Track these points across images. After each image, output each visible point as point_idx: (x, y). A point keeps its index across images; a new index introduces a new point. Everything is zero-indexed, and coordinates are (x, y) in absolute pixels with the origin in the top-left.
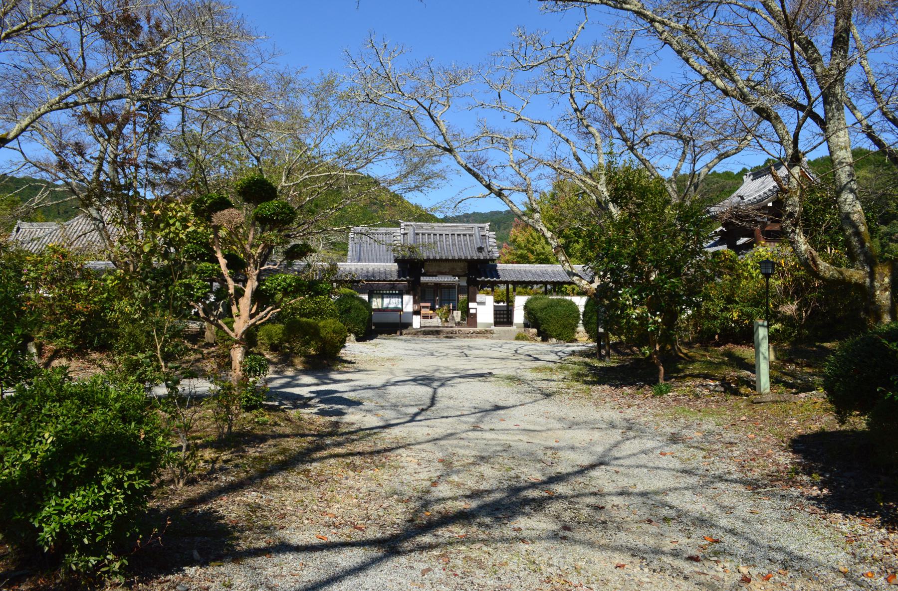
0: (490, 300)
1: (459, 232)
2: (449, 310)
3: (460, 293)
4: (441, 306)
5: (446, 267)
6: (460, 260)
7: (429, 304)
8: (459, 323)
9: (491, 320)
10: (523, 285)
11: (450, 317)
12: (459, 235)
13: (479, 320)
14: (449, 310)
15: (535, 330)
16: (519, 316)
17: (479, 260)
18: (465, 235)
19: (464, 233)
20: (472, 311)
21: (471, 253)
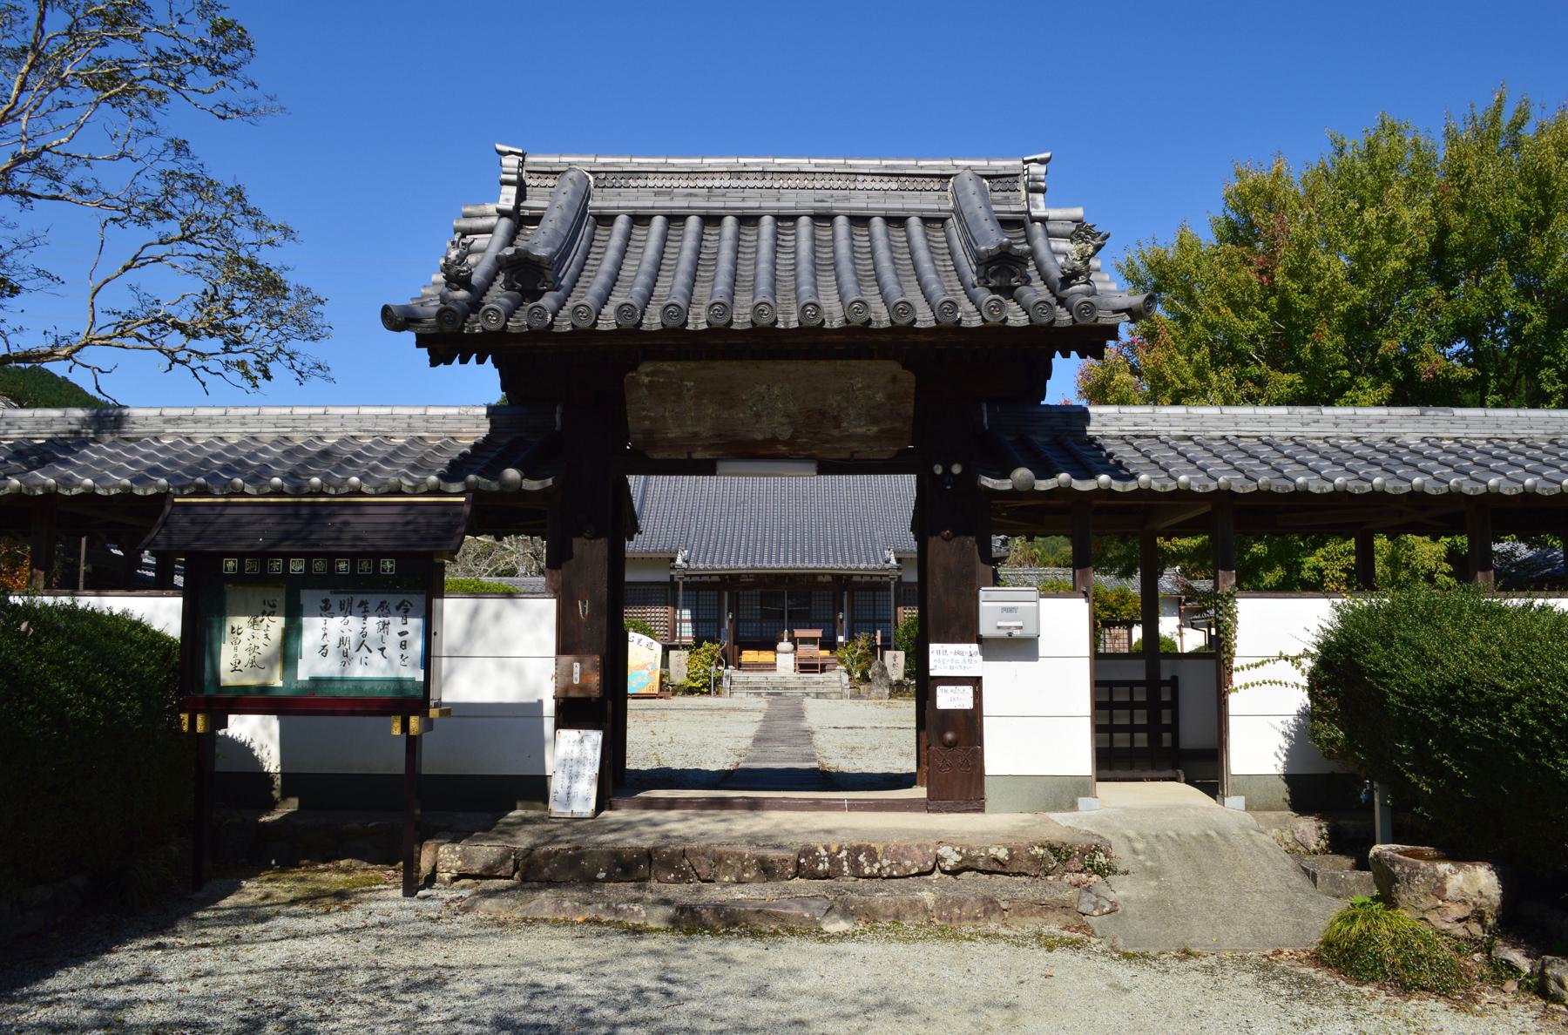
0: (1065, 623)
1: (859, 203)
2: (873, 649)
3: (901, 601)
4: (851, 637)
5: (773, 394)
6: (857, 341)
7: (818, 633)
8: (899, 683)
9: (1073, 751)
10: (1260, 534)
11: (875, 668)
12: (859, 221)
13: (1004, 753)
14: (873, 649)
15: (1478, 882)
16: (1263, 723)
17: (997, 332)
18: (896, 221)
19: (895, 205)
20: (949, 699)
21: (933, 289)
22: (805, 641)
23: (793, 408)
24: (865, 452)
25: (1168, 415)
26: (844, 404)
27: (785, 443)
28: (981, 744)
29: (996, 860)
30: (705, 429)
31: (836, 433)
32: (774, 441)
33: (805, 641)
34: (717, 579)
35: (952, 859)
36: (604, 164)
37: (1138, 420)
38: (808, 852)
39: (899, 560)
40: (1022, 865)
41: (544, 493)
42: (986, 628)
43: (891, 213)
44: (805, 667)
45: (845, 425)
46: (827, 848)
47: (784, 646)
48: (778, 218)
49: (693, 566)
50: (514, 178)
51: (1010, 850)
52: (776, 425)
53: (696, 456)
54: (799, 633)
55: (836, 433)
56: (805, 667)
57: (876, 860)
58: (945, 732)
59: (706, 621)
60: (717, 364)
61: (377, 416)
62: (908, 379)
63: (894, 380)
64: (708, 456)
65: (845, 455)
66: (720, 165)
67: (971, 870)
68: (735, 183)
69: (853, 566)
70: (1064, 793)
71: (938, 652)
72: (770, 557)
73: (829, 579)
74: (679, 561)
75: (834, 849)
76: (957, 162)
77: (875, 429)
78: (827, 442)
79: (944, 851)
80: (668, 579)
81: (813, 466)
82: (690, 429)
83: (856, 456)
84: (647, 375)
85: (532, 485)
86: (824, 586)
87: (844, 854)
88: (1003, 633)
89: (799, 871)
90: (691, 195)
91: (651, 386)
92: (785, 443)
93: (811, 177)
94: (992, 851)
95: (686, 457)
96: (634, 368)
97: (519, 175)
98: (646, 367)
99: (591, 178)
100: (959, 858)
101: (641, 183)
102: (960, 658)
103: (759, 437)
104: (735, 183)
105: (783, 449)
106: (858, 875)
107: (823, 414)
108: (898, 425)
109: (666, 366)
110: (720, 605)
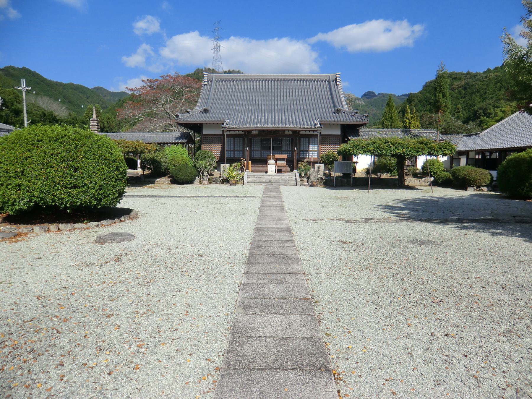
7: (285, 156)
22: (280, 159)
33: (280, 159)
44: (279, 171)
47: (272, 161)
49: (230, 126)
54: (277, 156)
56: (279, 171)
73: (290, 133)
86: (288, 136)
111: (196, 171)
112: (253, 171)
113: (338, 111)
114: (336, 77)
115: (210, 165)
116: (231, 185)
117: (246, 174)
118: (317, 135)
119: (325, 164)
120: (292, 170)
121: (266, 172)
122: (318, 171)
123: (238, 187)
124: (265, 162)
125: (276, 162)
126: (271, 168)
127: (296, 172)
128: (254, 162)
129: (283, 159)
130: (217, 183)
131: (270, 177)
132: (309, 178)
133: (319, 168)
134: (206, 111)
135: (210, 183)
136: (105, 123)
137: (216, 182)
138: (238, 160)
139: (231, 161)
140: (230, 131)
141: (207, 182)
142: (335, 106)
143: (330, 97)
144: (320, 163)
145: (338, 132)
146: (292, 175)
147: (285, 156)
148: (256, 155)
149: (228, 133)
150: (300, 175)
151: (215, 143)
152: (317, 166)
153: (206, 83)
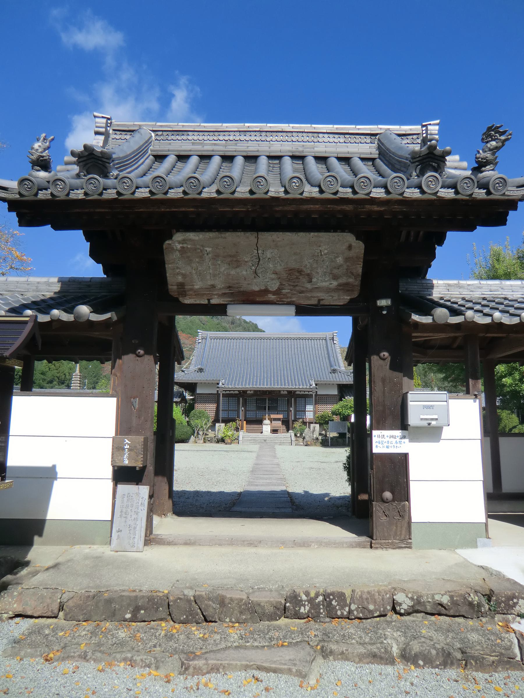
0: (464, 414)
7: (281, 416)
9: (469, 502)
22: (275, 419)
23: (279, 268)
24: (329, 300)
25: (511, 286)
26: (315, 265)
27: (274, 293)
28: (408, 499)
29: (441, 605)
30: (219, 283)
31: (309, 286)
32: (266, 291)
33: (275, 419)
34: (237, 392)
35: (405, 602)
36: (161, 126)
37: (493, 288)
38: (294, 598)
39: (316, 385)
40: (463, 610)
41: (106, 323)
42: (413, 420)
43: (339, 156)
44: (275, 431)
45: (314, 280)
46: (307, 594)
47: (267, 422)
48: (270, 157)
49: (226, 386)
50: (103, 130)
51: (452, 597)
52: (268, 281)
53: (213, 302)
54: (273, 416)
55: (309, 286)
56: (275, 431)
57: (346, 605)
58: (383, 491)
59: (232, 410)
60: (228, 234)
61: (18, 282)
62: (359, 247)
63: (350, 247)
64: (224, 303)
65: (314, 302)
66: (233, 127)
67: (418, 612)
68: (243, 138)
69: (297, 387)
70: (465, 535)
71: (379, 436)
72: (260, 383)
73: (286, 393)
74: (220, 384)
75: (312, 595)
76: (380, 126)
77: (335, 283)
78: (301, 292)
79: (400, 597)
80: (216, 392)
81: (292, 309)
82: (210, 283)
83: (322, 303)
84: (179, 243)
85: (95, 317)
86: (284, 396)
87: (321, 598)
88: (425, 423)
89: (284, 612)
90: (215, 144)
91: (183, 251)
92: (274, 293)
93: (289, 134)
94: (437, 597)
95: (206, 302)
96: (170, 237)
97: (106, 130)
98: (178, 236)
99: (153, 134)
100: (411, 603)
101: (185, 137)
102: (394, 440)
103: (257, 289)
104: (243, 138)
105: (271, 297)
106: (333, 617)
107: (300, 272)
108: (351, 280)
109: (191, 235)
110: (239, 404)
111: (192, 431)
112: (248, 431)
113: (334, 371)
114: (333, 336)
115: (206, 424)
116: (226, 444)
117: (241, 434)
118: (312, 395)
119: (321, 425)
120: (288, 430)
121: (262, 433)
122: (314, 431)
123: (234, 446)
124: (260, 422)
125: (271, 422)
126: (267, 427)
127: (292, 433)
128: (249, 422)
129: (278, 419)
130: (211, 442)
131: (265, 437)
132: (304, 438)
133: (314, 428)
134: (201, 370)
135: (205, 442)
136: (67, 374)
137: (211, 441)
138: (234, 420)
139: (226, 421)
140: (226, 391)
141: (202, 441)
142: (331, 366)
143: (326, 356)
144: (316, 423)
145: (335, 392)
146: (288, 435)
147: (281, 416)
148: (251, 415)
149: (224, 392)
150: (296, 435)
151: (209, 403)
152: (312, 426)
153: (200, 341)
